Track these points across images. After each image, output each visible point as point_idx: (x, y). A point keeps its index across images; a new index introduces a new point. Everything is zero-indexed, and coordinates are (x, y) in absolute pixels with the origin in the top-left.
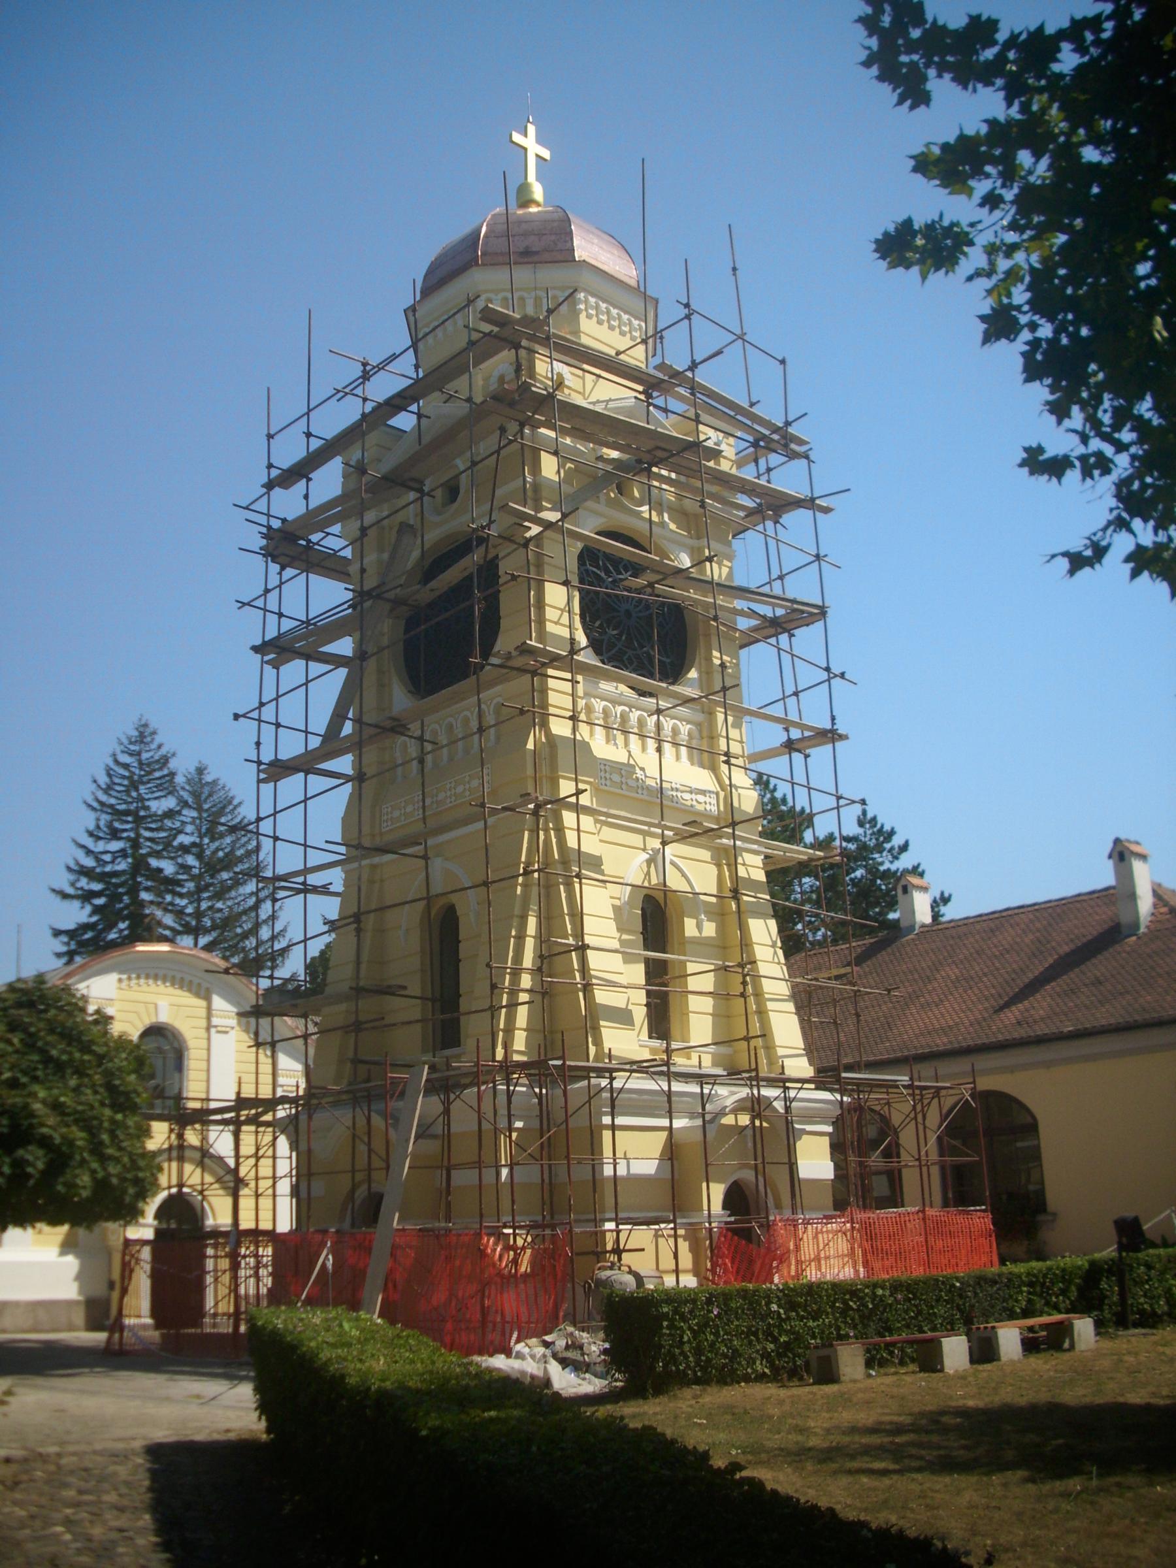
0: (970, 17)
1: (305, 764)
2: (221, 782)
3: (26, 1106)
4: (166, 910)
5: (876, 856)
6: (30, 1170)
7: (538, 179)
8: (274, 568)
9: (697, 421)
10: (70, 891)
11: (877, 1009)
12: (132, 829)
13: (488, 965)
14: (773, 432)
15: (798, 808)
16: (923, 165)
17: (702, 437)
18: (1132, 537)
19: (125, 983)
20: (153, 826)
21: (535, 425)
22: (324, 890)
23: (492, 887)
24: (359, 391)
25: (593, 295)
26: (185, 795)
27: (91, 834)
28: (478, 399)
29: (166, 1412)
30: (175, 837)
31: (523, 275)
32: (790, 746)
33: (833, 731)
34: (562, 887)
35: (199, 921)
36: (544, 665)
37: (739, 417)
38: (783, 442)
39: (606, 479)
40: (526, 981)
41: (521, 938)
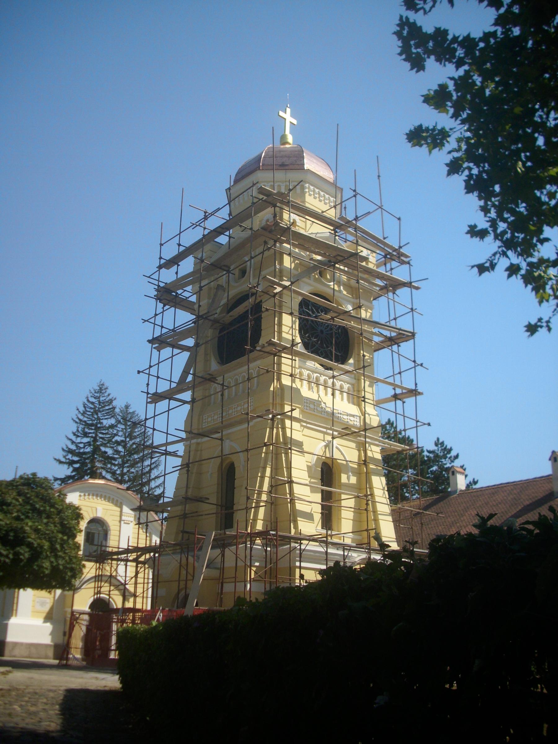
0: (436, 28)
1: (168, 395)
2: (136, 413)
3: (22, 527)
4: (107, 472)
5: (443, 460)
6: (22, 557)
7: (290, 133)
8: (160, 305)
9: (357, 244)
10: (63, 460)
11: (437, 528)
12: (93, 433)
13: (246, 488)
14: (394, 251)
15: (407, 436)
16: (427, 99)
17: (359, 251)
18: (508, 259)
19: (83, 497)
20: (104, 432)
21: (282, 242)
22: (174, 454)
23: (250, 453)
24: (202, 225)
25: (312, 185)
26: (120, 418)
27: (74, 434)
28: (255, 229)
29: (80, 680)
30: (114, 437)
31: (280, 175)
32: (396, 397)
33: (416, 390)
34: (283, 455)
35: (122, 477)
36: (279, 351)
37: (378, 244)
38: (398, 256)
39: (315, 268)
40: (264, 497)
41: (263, 477)
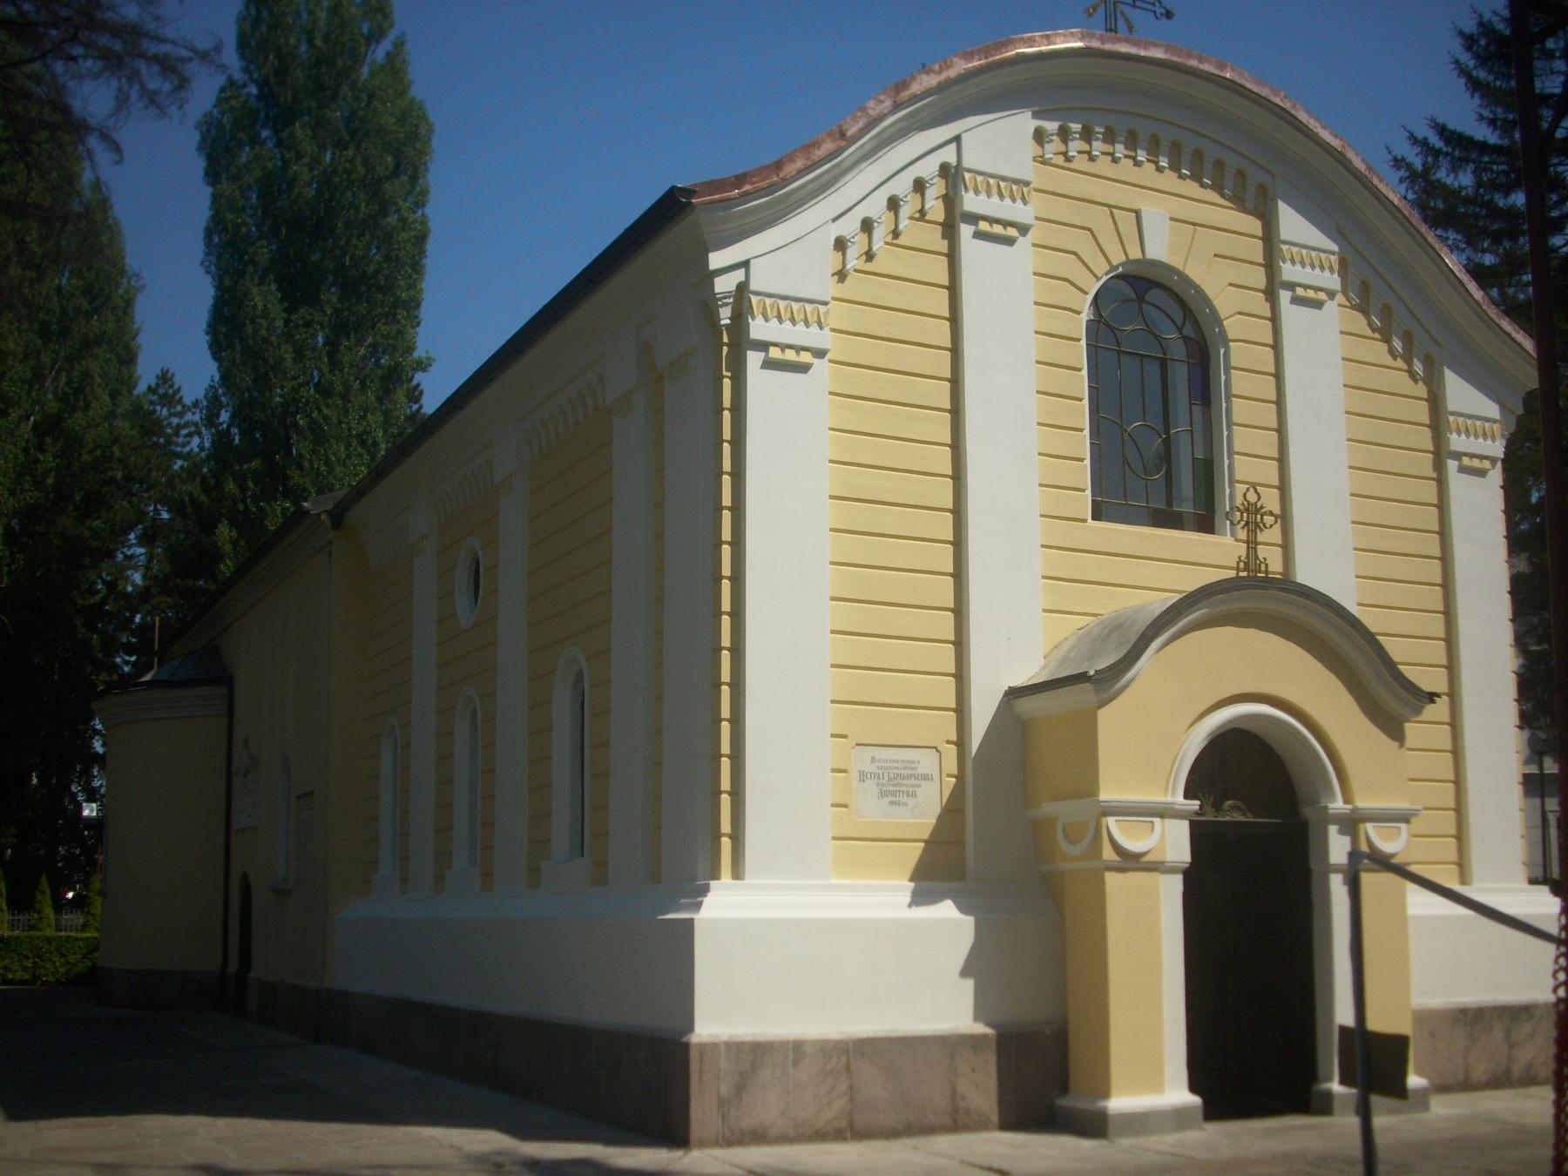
19: (1076, 146)
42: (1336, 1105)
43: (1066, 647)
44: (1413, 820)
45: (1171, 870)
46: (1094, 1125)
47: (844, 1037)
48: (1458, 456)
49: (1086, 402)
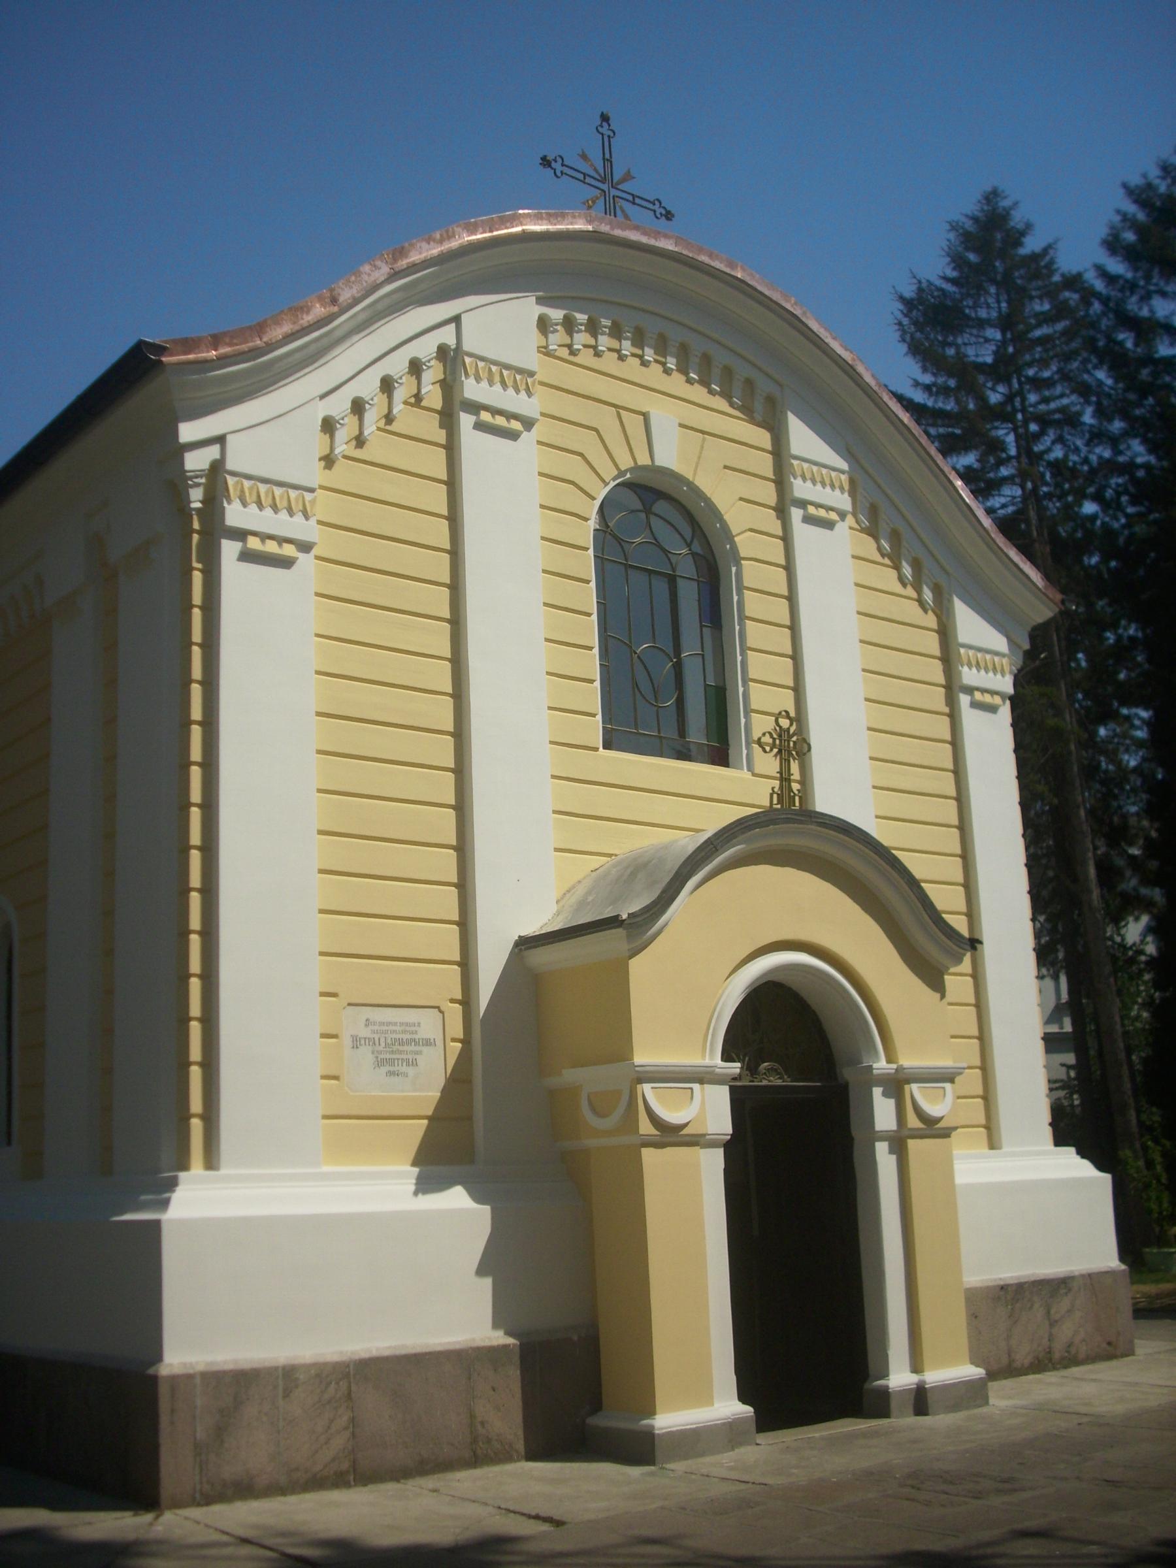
19: (558, 337)
42: (894, 1404)
43: (580, 891)
44: (957, 1079)
45: (712, 1144)
46: (639, 1449)
47: (344, 1358)
48: (970, 690)
49: (595, 617)
